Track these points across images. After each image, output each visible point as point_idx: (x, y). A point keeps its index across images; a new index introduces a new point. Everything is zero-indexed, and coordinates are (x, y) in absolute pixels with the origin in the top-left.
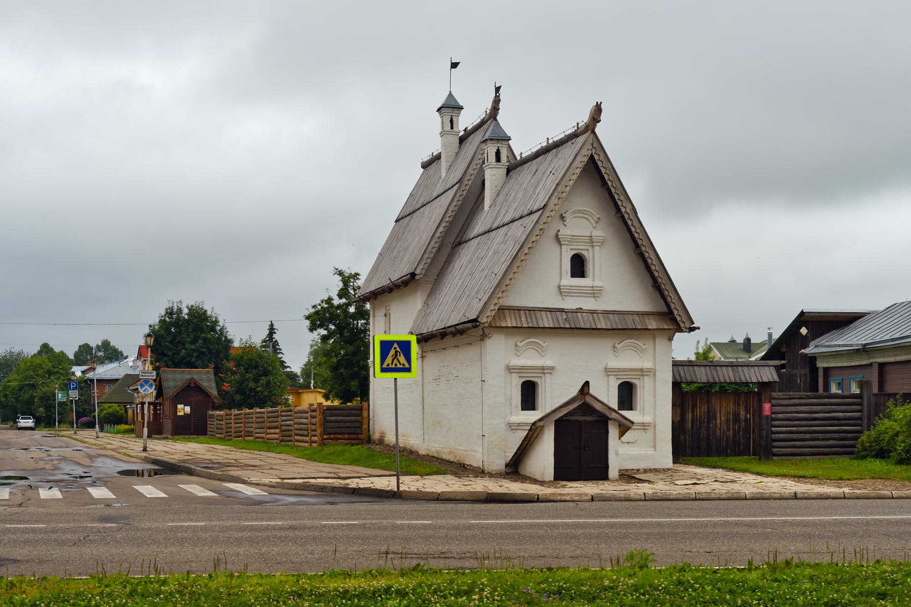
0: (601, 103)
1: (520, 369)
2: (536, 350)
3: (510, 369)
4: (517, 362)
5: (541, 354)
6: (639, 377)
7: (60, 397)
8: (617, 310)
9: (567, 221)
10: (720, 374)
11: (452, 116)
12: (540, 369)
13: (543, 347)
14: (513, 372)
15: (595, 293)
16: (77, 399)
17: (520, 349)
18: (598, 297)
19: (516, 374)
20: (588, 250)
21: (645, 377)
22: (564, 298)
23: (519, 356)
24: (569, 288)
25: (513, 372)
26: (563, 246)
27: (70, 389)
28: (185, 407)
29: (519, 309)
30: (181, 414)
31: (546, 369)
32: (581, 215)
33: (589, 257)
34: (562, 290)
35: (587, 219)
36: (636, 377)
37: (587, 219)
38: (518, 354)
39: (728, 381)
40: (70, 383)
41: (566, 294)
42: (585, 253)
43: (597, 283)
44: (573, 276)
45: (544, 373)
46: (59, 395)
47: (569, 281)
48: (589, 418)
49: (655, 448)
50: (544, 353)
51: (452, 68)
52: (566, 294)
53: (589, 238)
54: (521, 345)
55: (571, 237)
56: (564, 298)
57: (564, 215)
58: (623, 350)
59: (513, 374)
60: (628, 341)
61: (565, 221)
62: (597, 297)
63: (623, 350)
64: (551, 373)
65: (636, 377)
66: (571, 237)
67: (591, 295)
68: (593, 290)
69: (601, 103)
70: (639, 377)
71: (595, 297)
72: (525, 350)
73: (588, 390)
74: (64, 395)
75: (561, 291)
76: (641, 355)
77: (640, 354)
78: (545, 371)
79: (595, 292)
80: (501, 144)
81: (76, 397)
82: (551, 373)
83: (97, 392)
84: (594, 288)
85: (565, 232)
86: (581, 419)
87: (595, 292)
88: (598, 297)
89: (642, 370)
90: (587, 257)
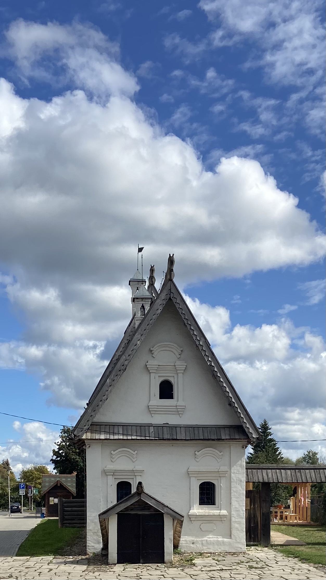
0: (173, 255)
1: (114, 473)
2: (213, 457)
3: (105, 473)
4: (111, 467)
5: (132, 460)
6: (217, 478)
7: (34, 492)
8: (198, 424)
9: (155, 353)
10: (283, 475)
11: (138, 287)
12: (131, 472)
13: (134, 455)
14: (109, 475)
15: (178, 411)
16: (24, 494)
17: (114, 456)
18: (182, 414)
19: (194, 478)
20: (174, 376)
21: (222, 478)
22: (153, 415)
23: (113, 462)
24: (156, 407)
25: (109, 475)
26: (151, 374)
27: (20, 488)
28: (55, 499)
29: (114, 425)
30: (52, 503)
31: (136, 472)
32: (167, 349)
33: (174, 383)
34: (150, 409)
35: (172, 352)
36: (214, 478)
37: (172, 352)
38: (113, 460)
39: (300, 481)
40: (20, 484)
41: (154, 412)
42: (171, 379)
43: (181, 403)
44: (161, 397)
45: (136, 476)
46: (34, 490)
47: (156, 401)
48: (146, 513)
49: (231, 536)
50: (136, 459)
51: (139, 252)
52: (154, 412)
53: (174, 367)
54: (114, 454)
55: (157, 366)
56: (153, 415)
57: (151, 349)
58: (203, 456)
59: (109, 477)
60: (208, 449)
61: (153, 354)
62: (181, 414)
63: (203, 456)
64: (141, 476)
65: (214, 478)
66: (157, 366)
67: (176, 413)
68: (177, 409)
69: (173, 255)
70: (217, 478)
71: (179, 414)
72: (119, 457)
73: (141, 489)
74: (37, 491)
75: (149, 410)
76: (219, 461)
77: (217, 459)
78: (136, 474)
79: (178, 410)
80: (145, 301)
81: (23, 493)
82: (141, 476)
83: (10, 489)
84: (178, 407)
85: (152, 363)
86: (140, 513)
87: (178, 410)
88: (182, 414)
89: (133, 471)
90: (173, 382)
